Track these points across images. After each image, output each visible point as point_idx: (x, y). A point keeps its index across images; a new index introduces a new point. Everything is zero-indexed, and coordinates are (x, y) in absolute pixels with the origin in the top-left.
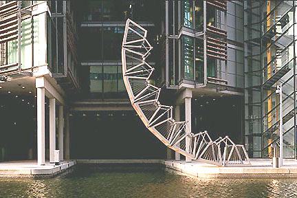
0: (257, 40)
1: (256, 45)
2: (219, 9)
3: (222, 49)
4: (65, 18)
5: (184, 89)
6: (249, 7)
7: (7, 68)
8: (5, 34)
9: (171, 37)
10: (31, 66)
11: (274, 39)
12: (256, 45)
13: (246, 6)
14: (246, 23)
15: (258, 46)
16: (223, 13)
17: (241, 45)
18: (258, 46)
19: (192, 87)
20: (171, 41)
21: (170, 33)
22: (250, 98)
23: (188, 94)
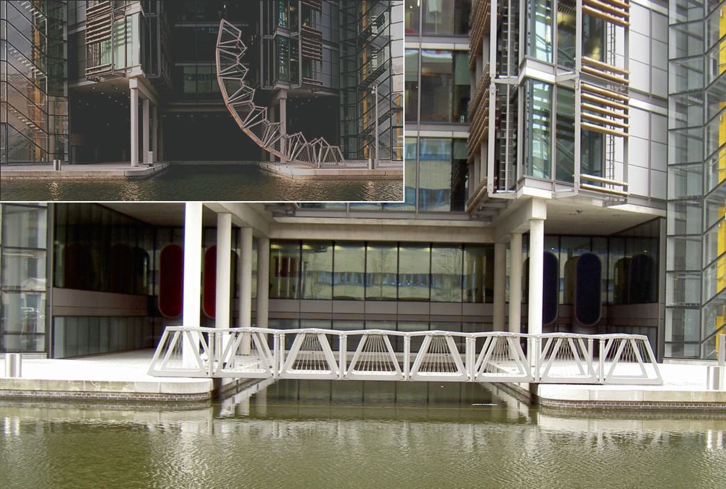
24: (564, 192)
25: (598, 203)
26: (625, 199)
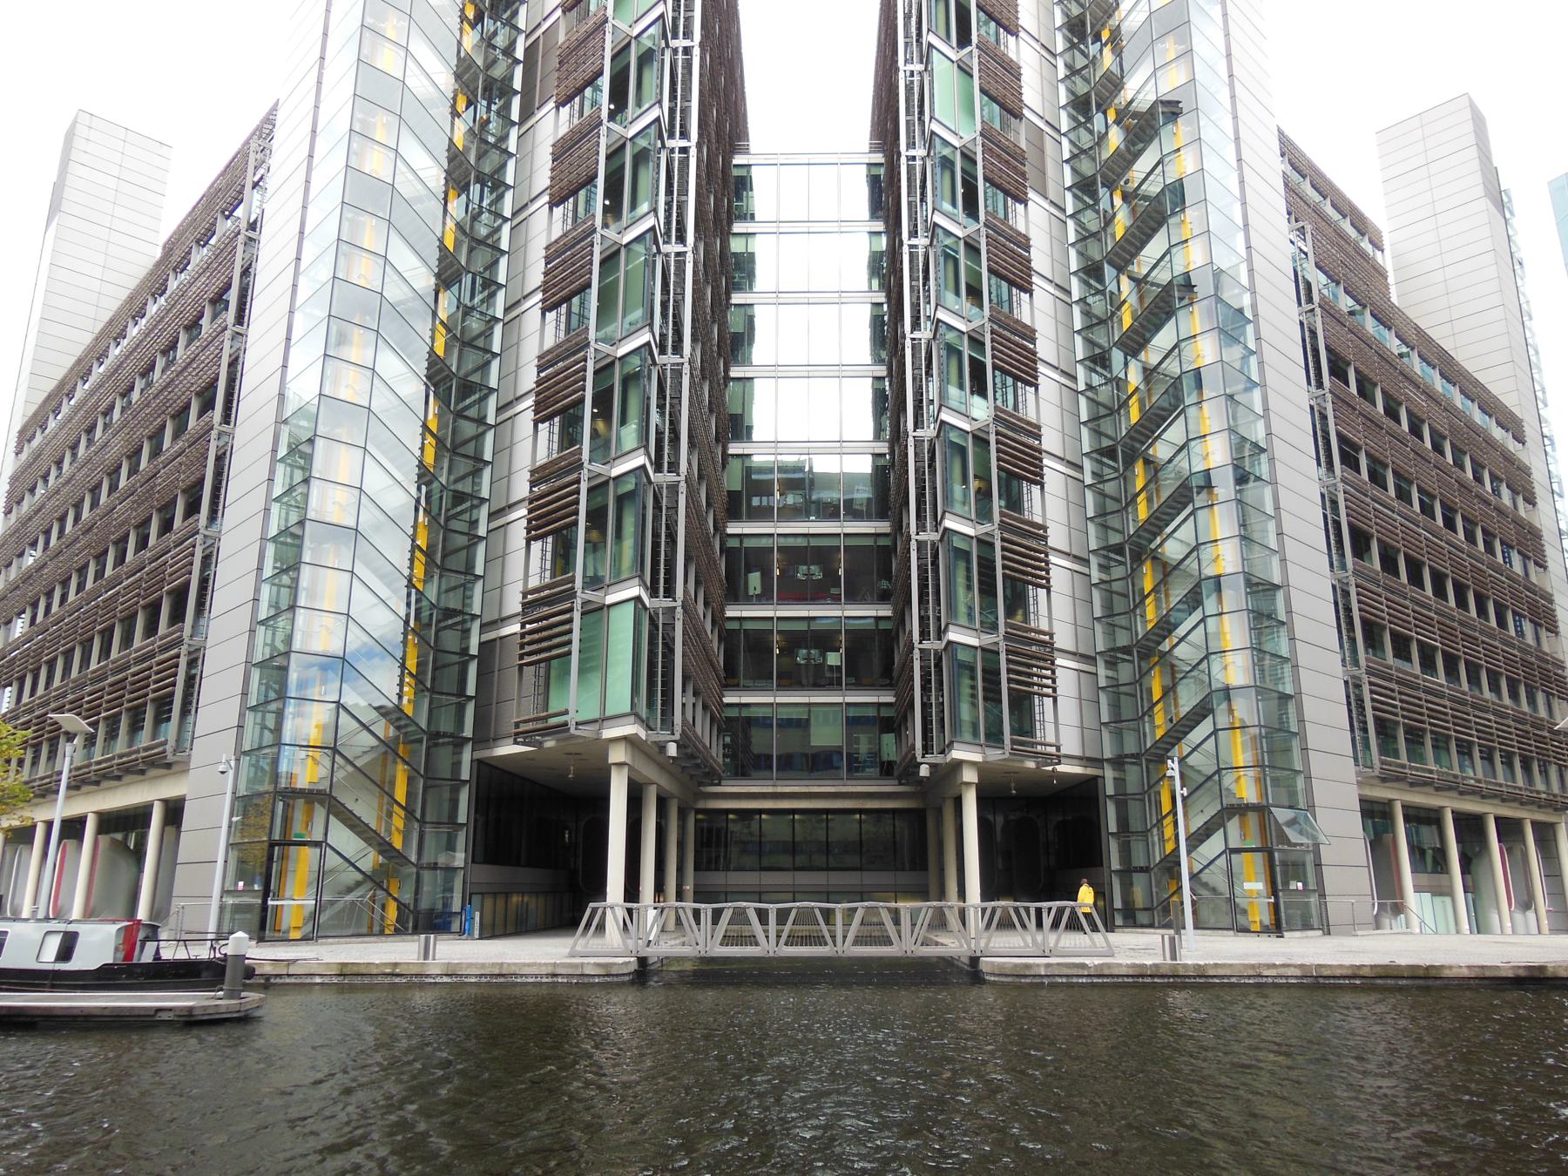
0: (1126, 650)
1: (1124, 660)
2: (1028, 480)
3: (1045, 681)
4: (679, 610)
5: (959, 764)
6: (1104, 577)
7: (545, 718)
8: (545, 644)
9: (926, 645)
10: (596, 715)
11: (1166, 646)
12: (1124, 660)
13: (1096, 575)
14: (1098, 613)
15: (1128, 661)
16: (1048, 702)
17: (1089, 659)
18: (1128, 661)
19: (977, 758)
20: (921, 545)
21: (924, 635)
22: (1120, 782)
23: (970, 776)
24: (995, 755)
25: (1031, 764)
26: (1059, 759)
